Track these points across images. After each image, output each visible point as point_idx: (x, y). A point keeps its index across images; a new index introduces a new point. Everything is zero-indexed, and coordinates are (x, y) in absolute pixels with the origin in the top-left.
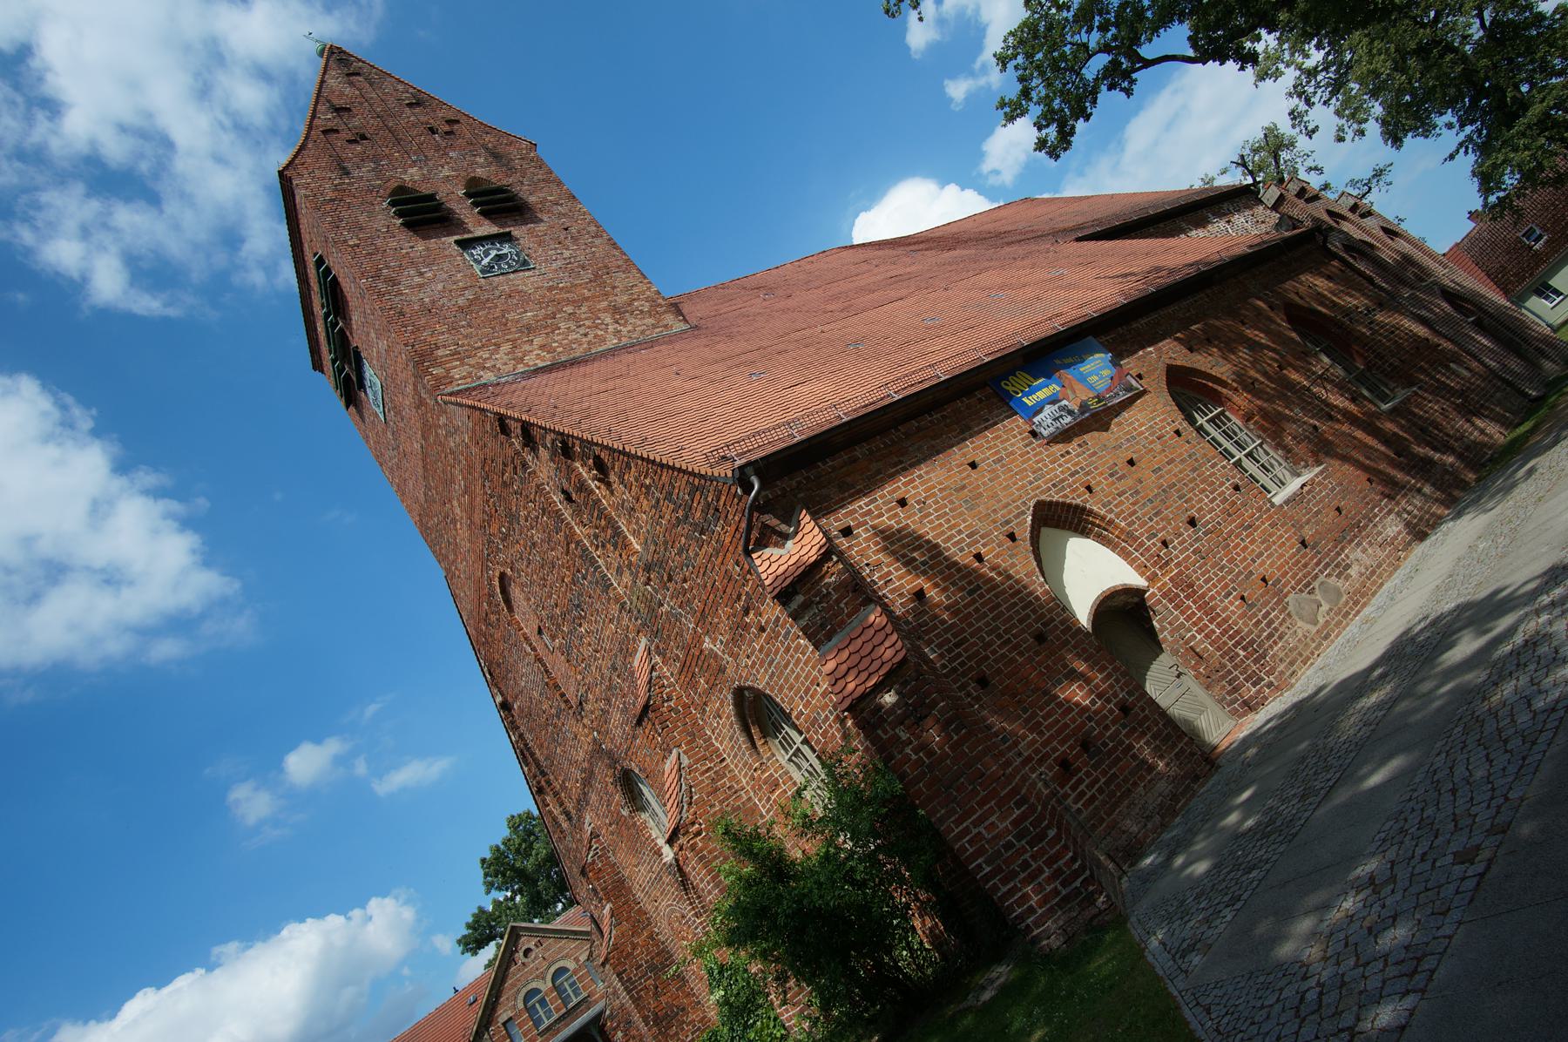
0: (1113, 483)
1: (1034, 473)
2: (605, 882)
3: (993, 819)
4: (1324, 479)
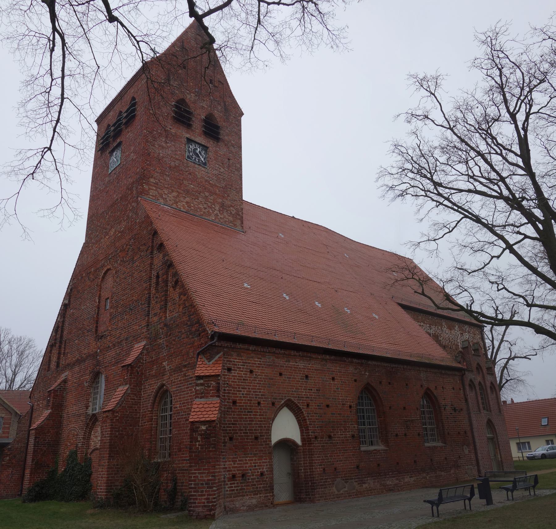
0: (316, 409)
1: (296, 389)
2: (56, 401)
3: (204, 475)
4: (383, 453)
